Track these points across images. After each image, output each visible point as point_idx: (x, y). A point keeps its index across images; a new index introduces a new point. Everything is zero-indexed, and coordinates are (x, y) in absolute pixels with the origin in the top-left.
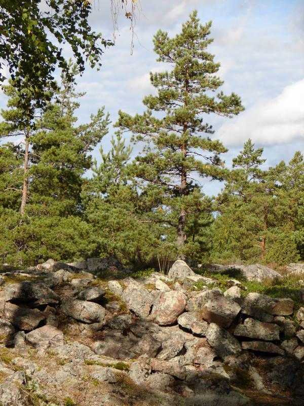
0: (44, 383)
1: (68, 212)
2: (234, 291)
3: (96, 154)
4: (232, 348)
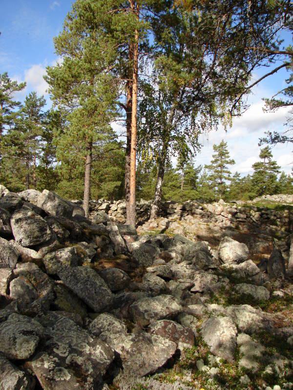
0: (189, 229)
1: (193, 189)
2: (235, 206)
3: (199, 175)
4: (235, 220)
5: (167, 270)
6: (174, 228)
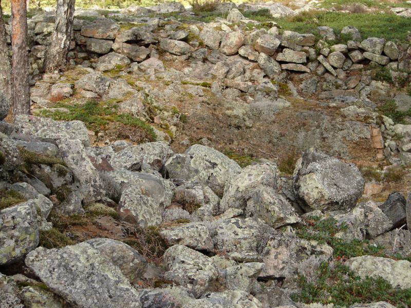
5: (203, 235)
6: (120, 97)
